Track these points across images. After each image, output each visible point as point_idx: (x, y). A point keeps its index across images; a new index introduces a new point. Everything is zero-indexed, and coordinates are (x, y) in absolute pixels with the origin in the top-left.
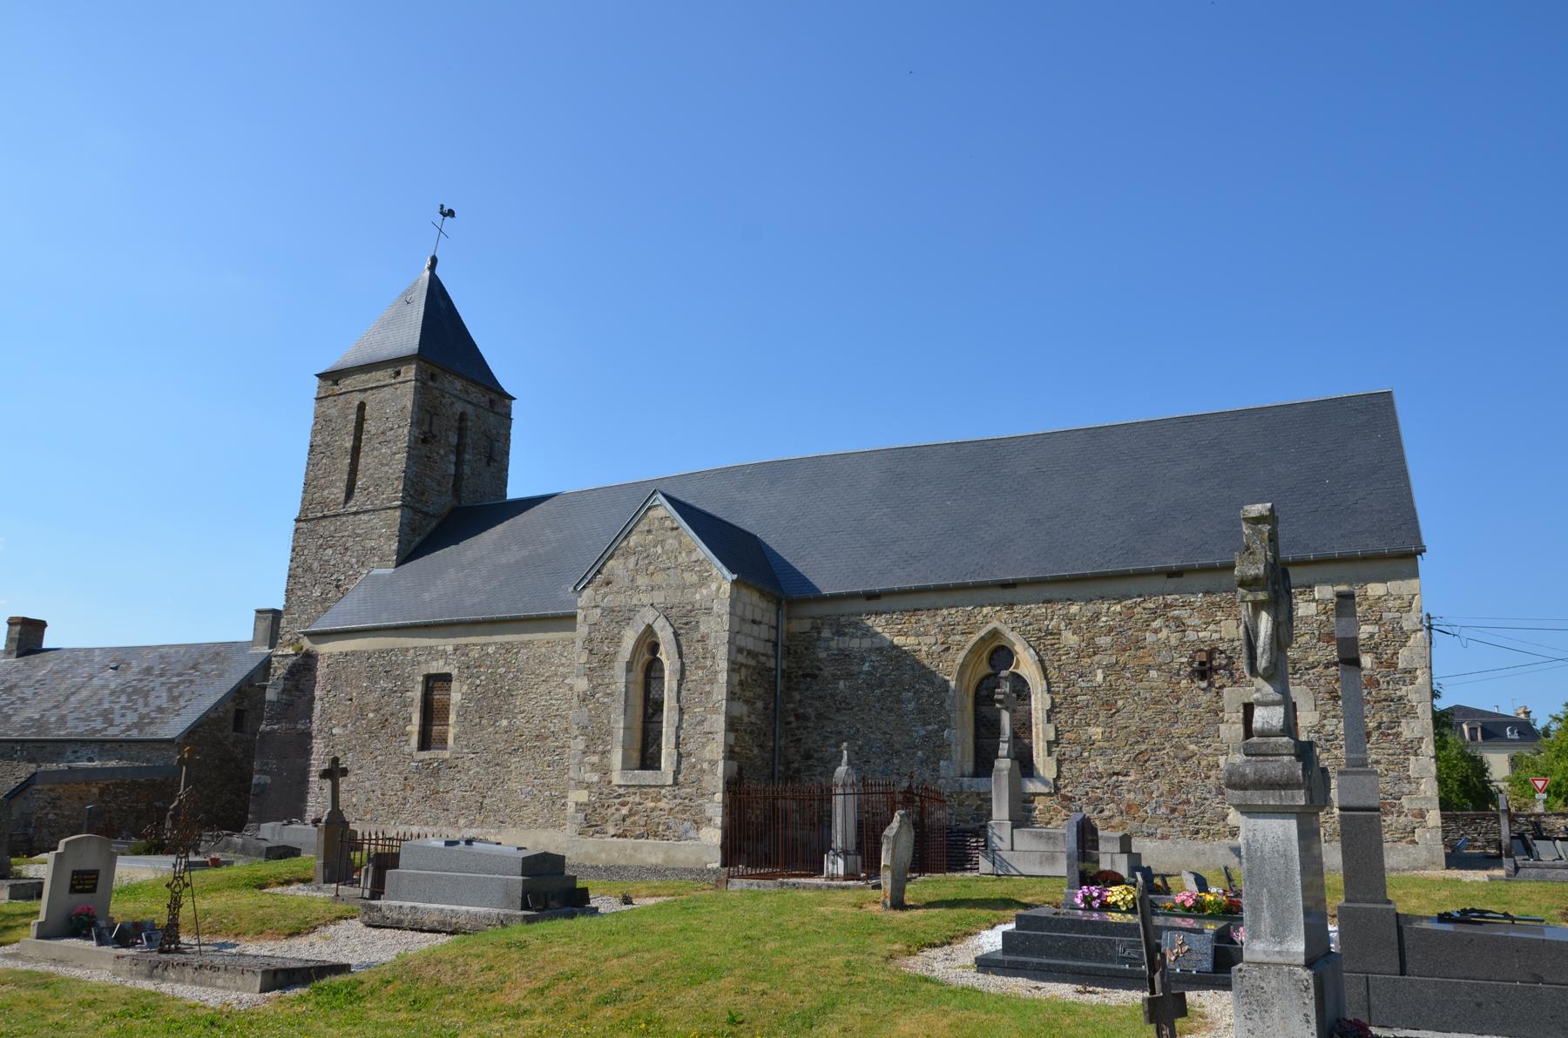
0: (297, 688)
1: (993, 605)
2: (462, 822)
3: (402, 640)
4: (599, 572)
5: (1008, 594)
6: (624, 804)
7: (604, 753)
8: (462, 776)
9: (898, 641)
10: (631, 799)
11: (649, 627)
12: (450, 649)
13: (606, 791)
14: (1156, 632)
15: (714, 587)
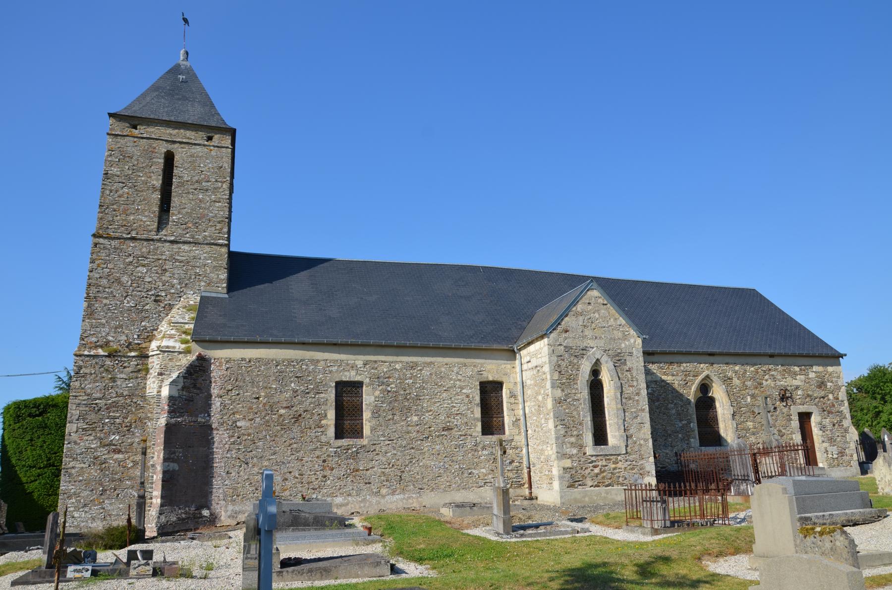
0: (195, 386)
1: (705, 363)
2: (384, 491)
3: (297, 352)
4: (559, 324)
5: (712, 359)
6: (595, 467)
7: (578, 436)
8: (380, 457)
9: (664, 377)
10: (600, 463)
11: (598, 360)
12: (360, 363)
13: (583, 460)
14: (766, 380)
15: (632, 341)
